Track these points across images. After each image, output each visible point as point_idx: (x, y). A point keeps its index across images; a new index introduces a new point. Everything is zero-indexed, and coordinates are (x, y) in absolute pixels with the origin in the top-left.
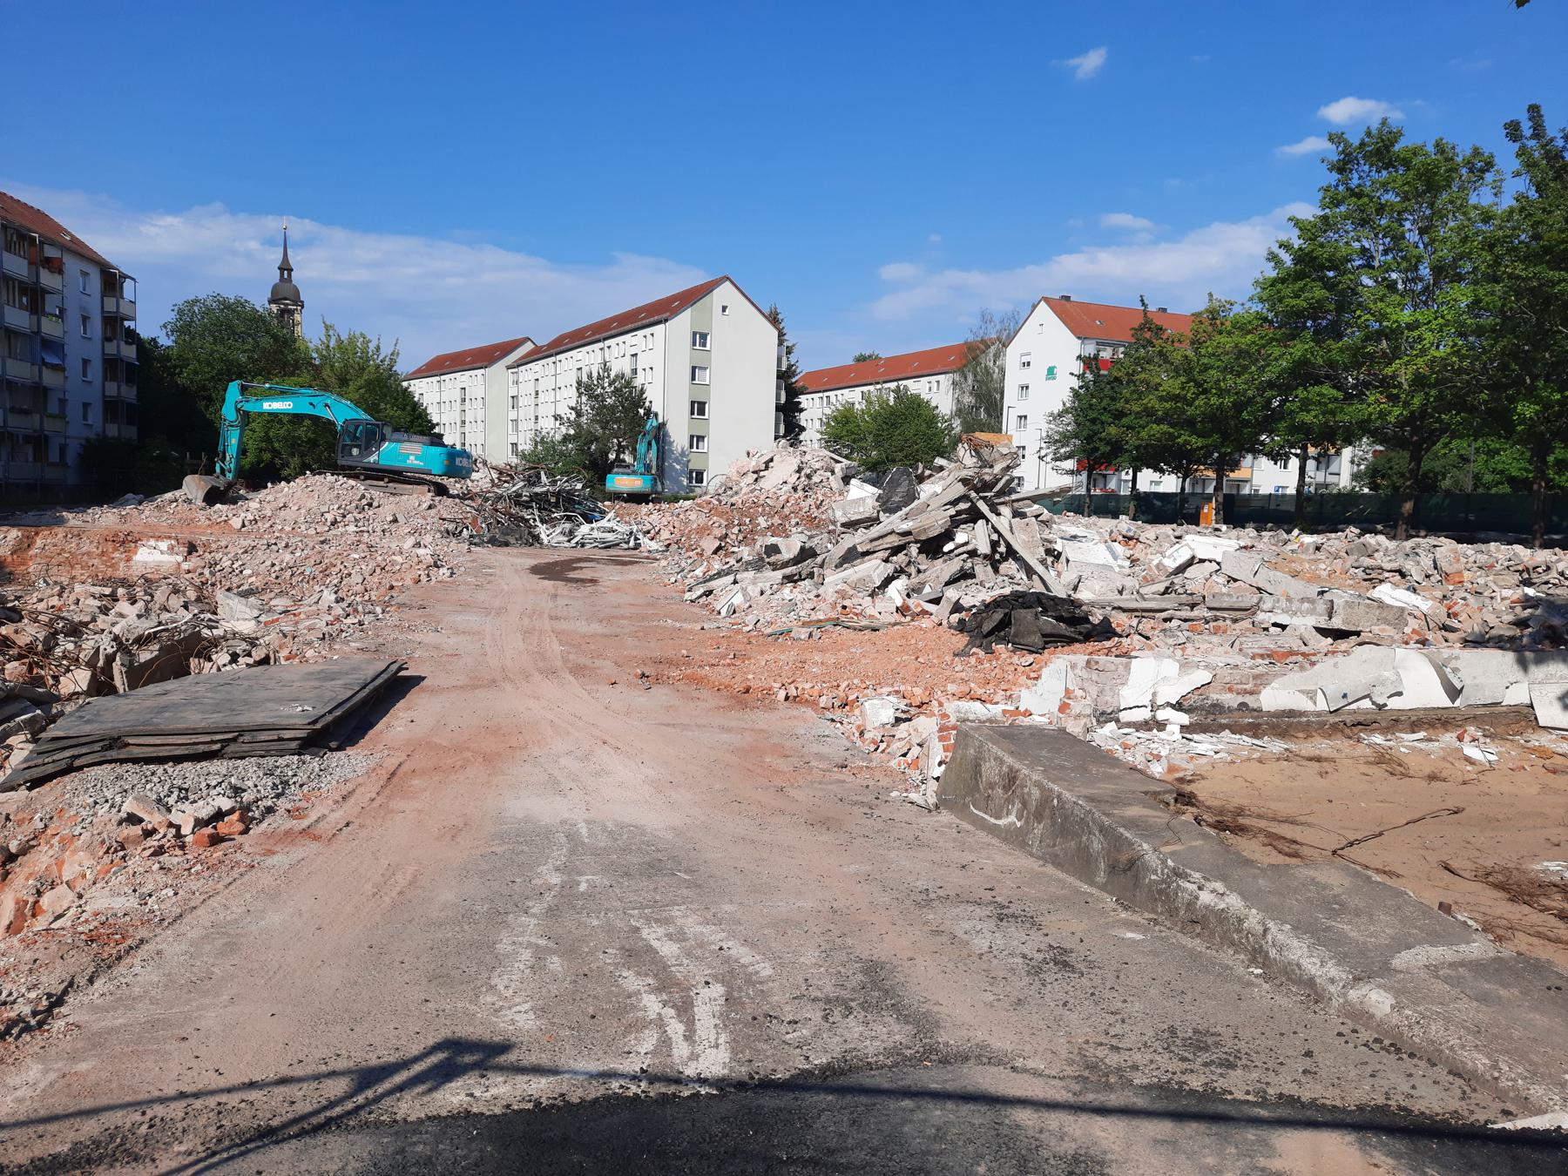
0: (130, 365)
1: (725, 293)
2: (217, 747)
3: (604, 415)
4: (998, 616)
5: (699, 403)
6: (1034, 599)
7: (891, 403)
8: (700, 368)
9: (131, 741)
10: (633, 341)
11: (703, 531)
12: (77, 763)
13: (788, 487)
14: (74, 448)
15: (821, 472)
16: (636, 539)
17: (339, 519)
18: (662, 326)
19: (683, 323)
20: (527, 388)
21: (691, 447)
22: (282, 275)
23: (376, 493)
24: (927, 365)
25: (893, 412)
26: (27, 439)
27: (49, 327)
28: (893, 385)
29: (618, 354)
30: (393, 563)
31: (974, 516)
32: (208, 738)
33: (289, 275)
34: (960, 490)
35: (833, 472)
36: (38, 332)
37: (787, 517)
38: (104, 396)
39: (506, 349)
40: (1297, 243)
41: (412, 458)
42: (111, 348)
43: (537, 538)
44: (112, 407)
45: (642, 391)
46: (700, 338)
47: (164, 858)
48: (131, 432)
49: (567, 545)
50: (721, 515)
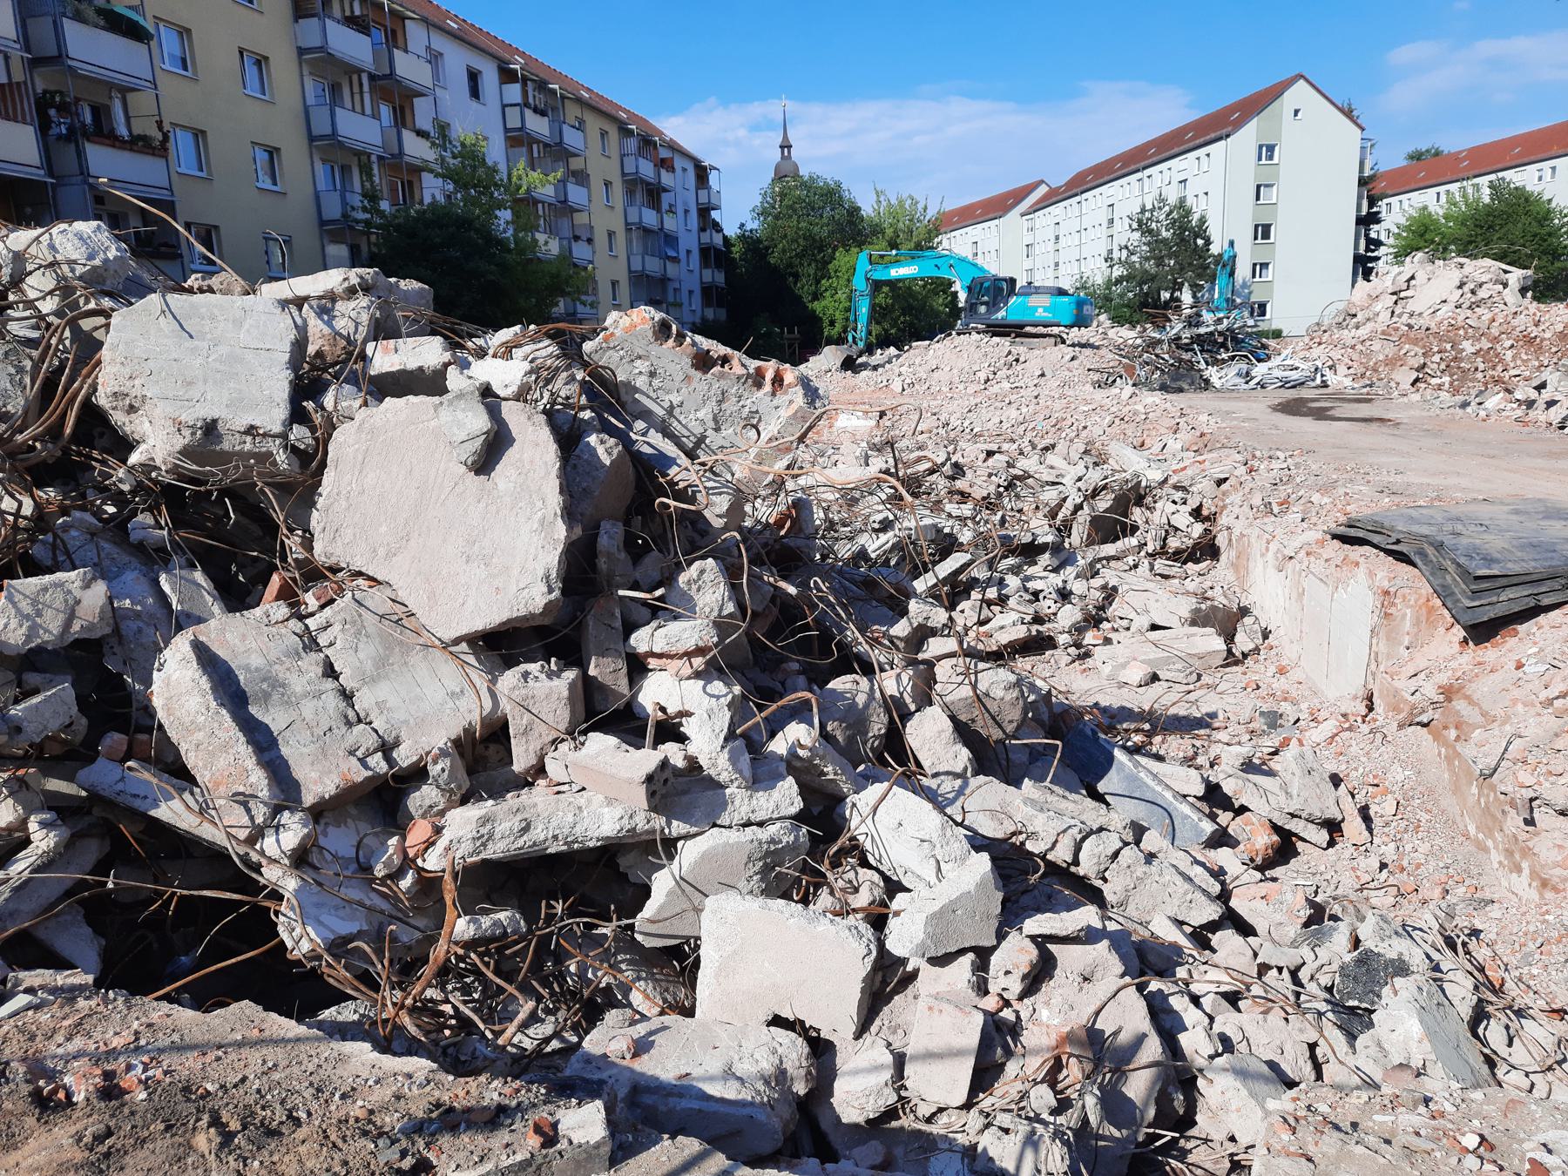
0: (717, 251)
1: (1299, 94)
3: (1158, 248)
5: (1263, 225)
7: (1487, 200)
8: (1266, 186)
10: (1183, 165)
11: (1391, 362)
12: (1546, 601)
13: (1449, 307)
15: (1490, 285)
16: (1322, 376)
17: (991, 377)
18: (1223, 143)
19: (1247, 136)
21: (1254, 276)
22: (783, 153)
23: (1022, 349)
25: (1489, 211)
27: (670, 223)
28: (1484, 181)
33: (789, 152)
35: (1505, 285)
36: (662, 229)
37: (1496, 340)
38: (702, 283)
39: (1019, 195)
41: (1040, 310)
42: (705, 238)
43: (1207, 381)
44: (708, 292)
45: (1203, 220)
49: (1246, 386)
50: (1415, 342)
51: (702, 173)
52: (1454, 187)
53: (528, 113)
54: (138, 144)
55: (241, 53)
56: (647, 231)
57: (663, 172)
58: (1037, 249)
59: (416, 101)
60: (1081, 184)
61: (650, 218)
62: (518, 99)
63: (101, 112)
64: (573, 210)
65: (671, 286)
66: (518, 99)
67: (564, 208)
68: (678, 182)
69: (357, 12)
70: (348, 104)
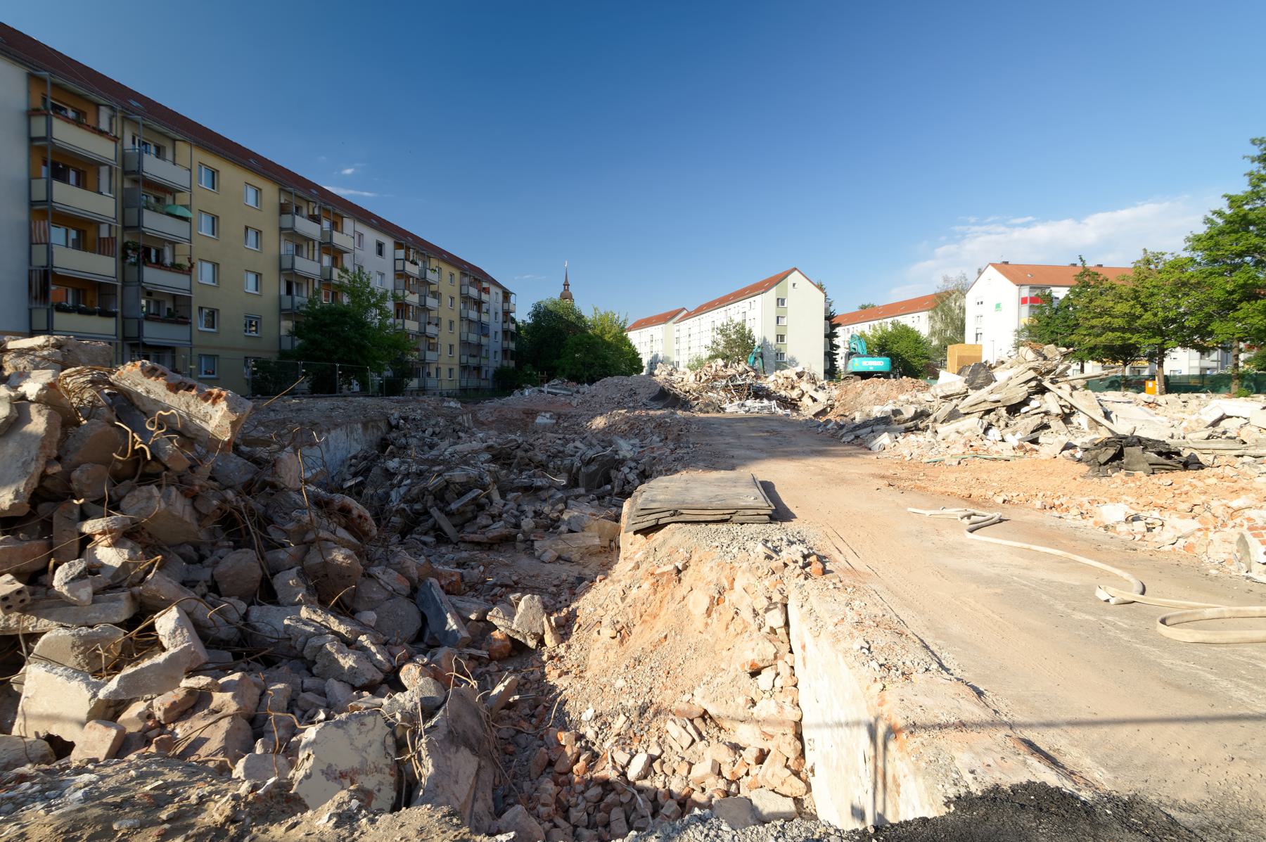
0: (512, 333)
2: (728, 517)
3: (730, 344)
4: (1111, 452)
6: (1135, 440)
7: (890, 330)
9: (684, 512)
10: (743, 305)
12: (661, 522)
14: (491, 371)
19: (772, 294)
20: (684, 333)
24: (911, 306)
25: (891, 334)
26: (475, 368)
27: (484, 318)
28: (889, 320)
29: (734, 313)
30: (666, 422)
31: (1042, 390)
32: (722, 512)
34: (1032, 374)
40: (1228, 212)
44: (505, 351)
45: (750, 331)
46: (781, 301)
47: (632, 565)
48: (512, 364)
51: (507, 295)
52: (876, 323)
53: (407, 264)
54: (176, 268)
55: (247, 228)
56: (470, 321)
57: (483, 294)
58: (681, 340)
59: (345, 255)
60: (700, 311)
61: (473, 315)
62: (403, 257)
63: (159, 253)
64: (429, 310)
65: (484, 349)
66: (403, 257)
67: (423, 308)
68: (493, 299)
69: (316, 213)
70: (305, 254)
